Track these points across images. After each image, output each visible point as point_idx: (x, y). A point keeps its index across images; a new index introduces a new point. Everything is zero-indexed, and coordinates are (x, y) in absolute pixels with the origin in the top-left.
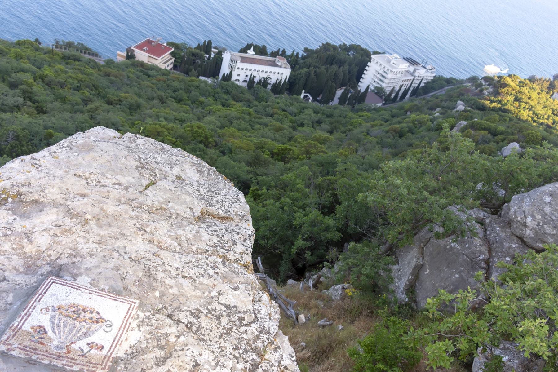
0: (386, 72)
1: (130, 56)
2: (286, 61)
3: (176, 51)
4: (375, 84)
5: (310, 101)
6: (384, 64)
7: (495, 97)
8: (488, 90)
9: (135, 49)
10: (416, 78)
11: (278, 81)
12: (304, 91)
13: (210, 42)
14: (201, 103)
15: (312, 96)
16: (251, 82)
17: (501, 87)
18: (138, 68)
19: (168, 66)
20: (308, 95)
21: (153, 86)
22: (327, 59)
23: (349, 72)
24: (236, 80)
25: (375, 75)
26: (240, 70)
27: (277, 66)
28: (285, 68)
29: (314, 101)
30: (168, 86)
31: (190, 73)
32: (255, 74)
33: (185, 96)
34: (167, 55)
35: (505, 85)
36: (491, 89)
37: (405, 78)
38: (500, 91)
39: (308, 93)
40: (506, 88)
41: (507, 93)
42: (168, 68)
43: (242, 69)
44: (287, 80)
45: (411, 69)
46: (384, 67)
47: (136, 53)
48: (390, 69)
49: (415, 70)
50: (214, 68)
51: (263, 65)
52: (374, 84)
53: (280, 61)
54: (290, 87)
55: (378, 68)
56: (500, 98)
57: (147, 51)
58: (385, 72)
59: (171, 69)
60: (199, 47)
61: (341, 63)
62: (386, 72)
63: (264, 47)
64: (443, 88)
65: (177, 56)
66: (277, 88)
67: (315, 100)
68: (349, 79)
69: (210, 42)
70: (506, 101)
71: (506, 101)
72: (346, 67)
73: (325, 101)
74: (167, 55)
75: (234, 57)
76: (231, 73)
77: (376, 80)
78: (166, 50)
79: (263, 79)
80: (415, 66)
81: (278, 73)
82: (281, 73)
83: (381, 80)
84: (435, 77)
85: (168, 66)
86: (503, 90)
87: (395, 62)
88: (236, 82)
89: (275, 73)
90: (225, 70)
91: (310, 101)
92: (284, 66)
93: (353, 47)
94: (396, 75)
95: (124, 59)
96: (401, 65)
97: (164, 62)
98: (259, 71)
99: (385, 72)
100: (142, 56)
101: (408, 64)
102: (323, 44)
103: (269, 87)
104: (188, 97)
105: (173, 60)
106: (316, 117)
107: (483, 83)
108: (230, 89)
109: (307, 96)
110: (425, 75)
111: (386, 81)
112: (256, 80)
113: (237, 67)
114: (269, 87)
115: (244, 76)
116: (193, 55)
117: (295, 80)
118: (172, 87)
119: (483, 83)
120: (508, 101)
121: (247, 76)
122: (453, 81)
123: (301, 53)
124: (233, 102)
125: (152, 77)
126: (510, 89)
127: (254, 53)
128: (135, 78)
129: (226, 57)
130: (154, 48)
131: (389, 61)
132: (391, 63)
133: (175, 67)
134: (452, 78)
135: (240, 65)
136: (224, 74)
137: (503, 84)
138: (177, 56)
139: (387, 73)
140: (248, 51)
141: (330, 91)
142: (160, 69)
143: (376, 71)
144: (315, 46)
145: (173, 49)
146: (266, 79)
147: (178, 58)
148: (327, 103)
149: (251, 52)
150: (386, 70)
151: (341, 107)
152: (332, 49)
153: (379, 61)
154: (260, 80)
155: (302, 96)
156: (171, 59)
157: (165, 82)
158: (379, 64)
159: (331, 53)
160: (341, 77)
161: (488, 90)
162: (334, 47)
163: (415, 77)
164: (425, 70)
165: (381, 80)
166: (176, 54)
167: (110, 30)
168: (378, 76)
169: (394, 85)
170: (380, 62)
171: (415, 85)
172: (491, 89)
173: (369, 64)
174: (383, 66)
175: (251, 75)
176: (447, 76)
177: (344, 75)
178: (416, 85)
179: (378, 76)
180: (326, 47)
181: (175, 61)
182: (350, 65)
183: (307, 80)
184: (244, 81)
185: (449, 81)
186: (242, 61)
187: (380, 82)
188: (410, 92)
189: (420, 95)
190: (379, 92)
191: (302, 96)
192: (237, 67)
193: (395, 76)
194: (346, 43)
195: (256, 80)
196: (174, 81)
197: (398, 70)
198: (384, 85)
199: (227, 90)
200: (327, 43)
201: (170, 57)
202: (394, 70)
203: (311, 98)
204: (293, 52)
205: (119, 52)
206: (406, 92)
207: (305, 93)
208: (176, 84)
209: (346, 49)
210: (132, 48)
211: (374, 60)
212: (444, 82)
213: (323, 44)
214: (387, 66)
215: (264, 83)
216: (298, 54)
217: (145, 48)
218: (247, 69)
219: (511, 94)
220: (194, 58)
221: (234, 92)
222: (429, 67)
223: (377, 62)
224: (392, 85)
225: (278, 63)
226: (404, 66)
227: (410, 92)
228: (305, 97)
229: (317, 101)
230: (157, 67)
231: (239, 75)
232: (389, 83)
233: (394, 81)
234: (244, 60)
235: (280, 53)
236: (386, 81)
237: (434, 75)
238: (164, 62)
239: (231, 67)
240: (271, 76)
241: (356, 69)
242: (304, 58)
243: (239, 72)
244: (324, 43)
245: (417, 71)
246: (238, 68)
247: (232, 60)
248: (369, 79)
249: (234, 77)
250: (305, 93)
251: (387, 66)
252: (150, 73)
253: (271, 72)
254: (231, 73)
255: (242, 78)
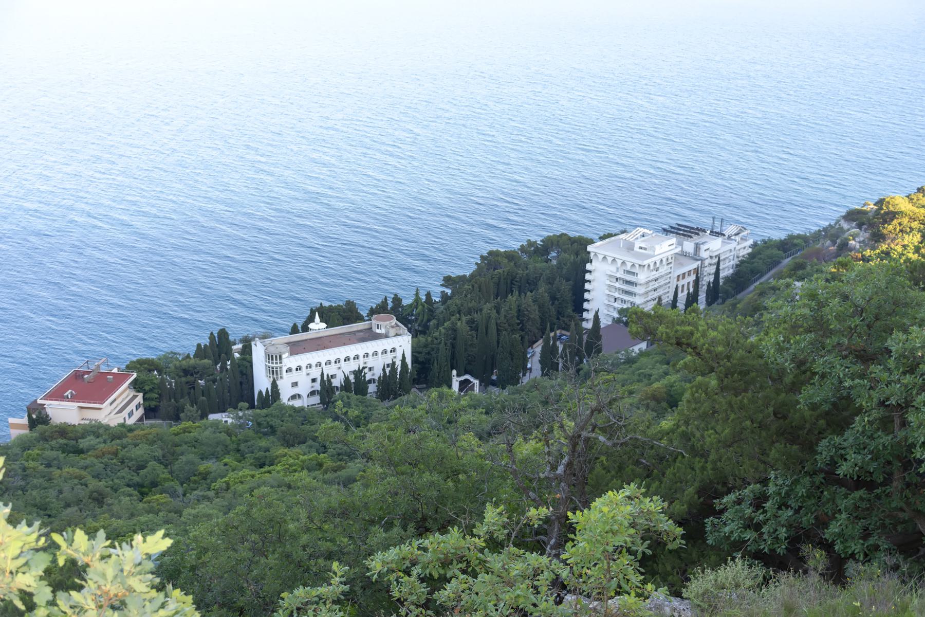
0: (630, 273)
1: (38, 418)
2: (394, 321)
3: (144, 376)
4: (618, 305)
5: (477, 389)
6: (621, 256)
7: (873, 248)
8: (857, 238)
9: (47, 402)
10: (706, 263)
11: (388, 370)
12: (454, 372)
13: (223, 333)
14: (205, 476)
15: (476, 378)
16: (326, 390)
17: (885, 222)
18: (53, 443)
19: (131, 414)
20: (467, 377)
21: (83, 473)
22: (498, 284)
23: (553, 298)
24: (293, 397)
25: (610, 286)
26: (294, 375)
27: (377, 337)
28: (397, 335)
29: (486, 386)
30: (122, 463)
31: (182, 415)
32: (329, 370)
33: (163, 473)
34: (124, 392)
35: (892, 215)
36: (864, 235)
37: (680, 271)
38: (885, 232)
39: (466, 373)
40: (895, 222)
41: (901, 231)
42: (131, 421)
43: (299, 369)
44: (409, 360)
45: (689, 246)
46: (624, 263)
47: (49, 411)
48: (638, 262)
49: (697, 247)
50: (238, 387)
51: (344, 344)
52: (616, 305)
53: (384, 324)
54: (424, 371)
55: (611, 269)
56: (884, 247)
57: (73, 399)
58: (629, 272)
59: (140, 419)
60: (201, 352)
61: (531, 284)
62: (630, 273)
63: (351, 305)
64: (779, 262)
65: (147, 388)
66: (392, 385)
67: (486, 383)
68: (559, 313)
69: (223, 333)
70: (899, 249)
71: (899, 249)
72: (542, 289)
73: (510, 379)
74: (124, 392)
75: (272, 350)
76: (274, 385)
77: (617, 295)
78: (119, 379)
79: (352, 378)
80: (695, 237)
81: (385, 352)
82: (395, 347)
83: (627, 293)
84: (755, 245)
85: (131, 414)
86: (890, 227)
87: (643, 245)
88: (297, 403)
89: (376, 353)
90: (262, 383)
91: (477, 389)
92: (392, 332)
93: (551, 243)
94: (657, 269)
95: (26, 432)
96: (657, 247)
97: (119, 409)
98: (337, 361)
99: (629, 272)
100: (66, 413)
101: (673, 240)
102: (482, 257)
103: (372, 388)
104: (171, 473)
105: (140, 398)
106: (487, 422)
107: (845, 226)
108: (275, 422)
109: (467, 381)
110: (725, 251)
111: (638, 290)
112: (336, 383)
113: (284, 369)
114: (372, 388)
115: (310, 384)
116: (186, 372)
117: (429, 353)
118: (131, 460)
119: (845, 226)
120: (905, 247)
121: (314, 380)
122: (796, 241)
123: (438, 291)
124: (282, 451)
125: (88, 450)
126: (905, 221)
127: (324, 325)
128: (42, 467)
129: (258, 353)
130: (88, 386)
131: (630, 247)
132: (636, 249)
133: (150, 412)
134: (791, 237)
135: (289, 361)
136: (260, 392)
137: (887, 213)
138: (147, 388)
139: (633, 274)
140: (311, 326)
141: (511, 353)
142: (107, 428)
143: (610, 276)
144: (466, 267)
145: (135, 375)
146: (358, 373)
147: (151, 390)
148: (515, 380)
149: (318, 326)
150: (628, 268)
151: (547, 382)
152: (506, 261)
153: (606, 253)
154: (347, 379)
155: (456, 386)
156: (135, 397)
157: (116, 454)
158: (610, 260)
159: (506, 267)
160: (535, 314)
161: (857, 238)
162: (510, 256)
163: (702, 260)
164: (719, 240)
165: (627, 293)
166: (143, 382)
167: (715, 187)
168: (617, 285)
169: (660, 292)
170: (611, 254)
171: (708, 278)
172: (864, 235)
173: (588, 266)
174: (619, 262)
175: (322, 375)
176: (778, 236)
177: (541, 307)
178: (712, 278)
179: (617, 285)
180: (491, 260)
181: (144, 399)
182: (550, 281)
183: (453, 346)
184: (312, 393)
185: (787, 246)
186: (292, 353)
187: (627, 298)
188: (702, 297)
189: (728, 295)
190: (630, 318)
191: (456, 386)
192: (284, 369)
193: (656, 274)
194: (533, 239)
195: (336, 383)
196: (136, 445)
197: (657, 259)
198: (638, 301)
199: (271, 427)
200: (491, 253)
201: (132, 393)
202: (646, 262)
203: (476, 382)
204: (417, 294)
205: (12, 420)
206: (692, 299)
207: (458, 375)
208: (141, 451)
209: (540, 250)
210: (39, 402)
211: (596, 254)
212: (775, 252)
213: (482, 257)
214: (630, 260)
215: (357, 384)
216: (428, 295)
217: (68, 393)
218: (310, 366)
219: (912, 229)
220: (190, 378)
221: (288, 425)
222: (730, 230)
223: (614, 260)
224: (656, 295)
225: (378, 331)
226: (667, 246)
227: (702, 297)
228: (461, 383)
229: (494, 384)
230: (100, 426)
231: (295, 384)
232: (647, 293)
233: (656, 285)
234: (296, 348)
235: (390, 305)
236: (638, 290)
237: (751, 242)
238: (119, 409)
239: (274, 373)
240: (370, 362)
241: (565, 287)
242: (445, 298)
243: (295, 376)
244: (485, 254)
245: (703, 247)
246: (289, 370)
247: (270, 357)
248: (601, 299)
249: (286, 393)
250: (458, 375)
251: (630, 260)
252: (83, 444)
253: (366, 355)
254: (274, 385)
255: (304, 388)
